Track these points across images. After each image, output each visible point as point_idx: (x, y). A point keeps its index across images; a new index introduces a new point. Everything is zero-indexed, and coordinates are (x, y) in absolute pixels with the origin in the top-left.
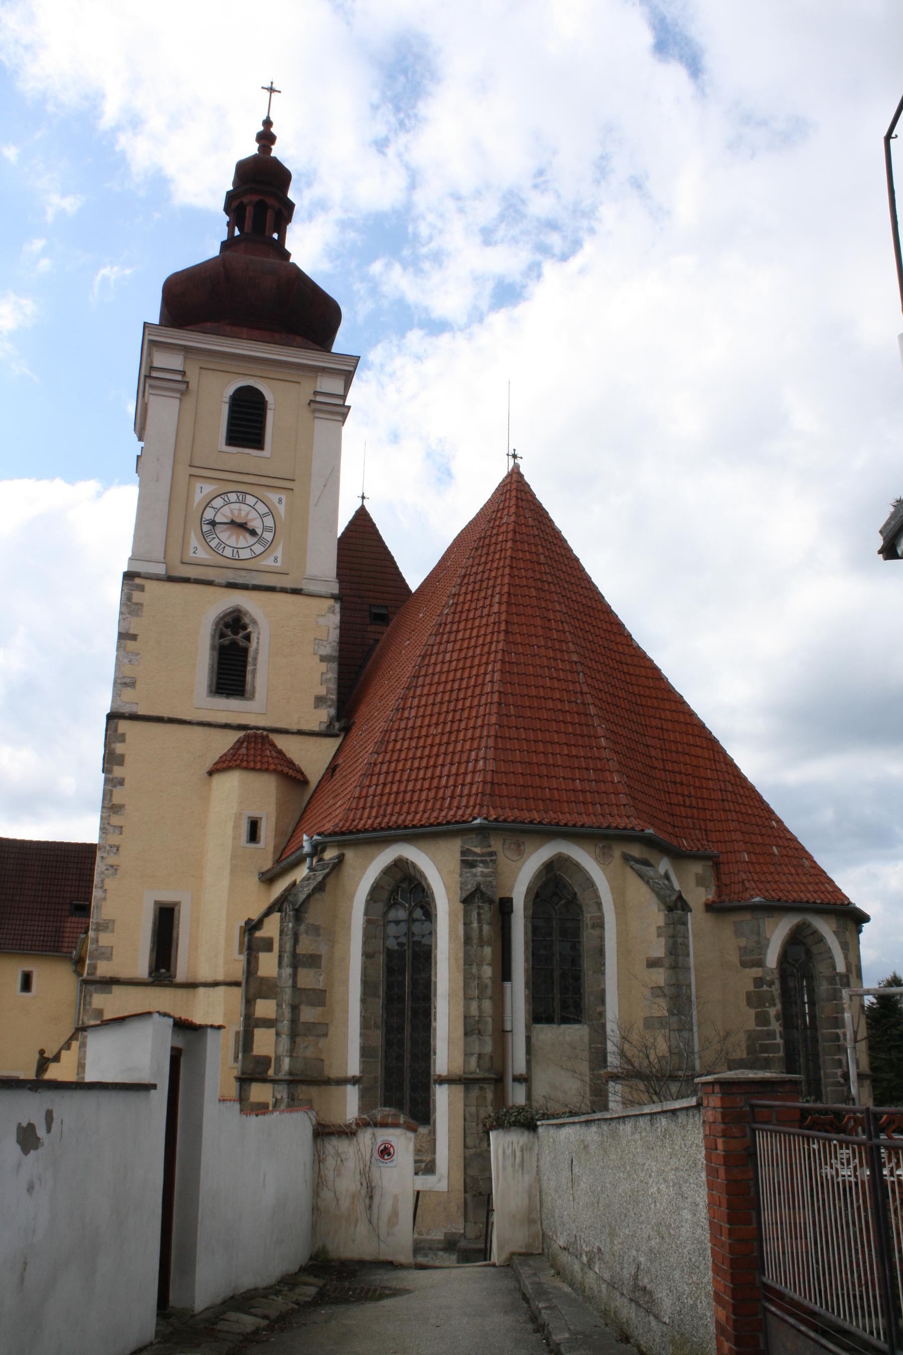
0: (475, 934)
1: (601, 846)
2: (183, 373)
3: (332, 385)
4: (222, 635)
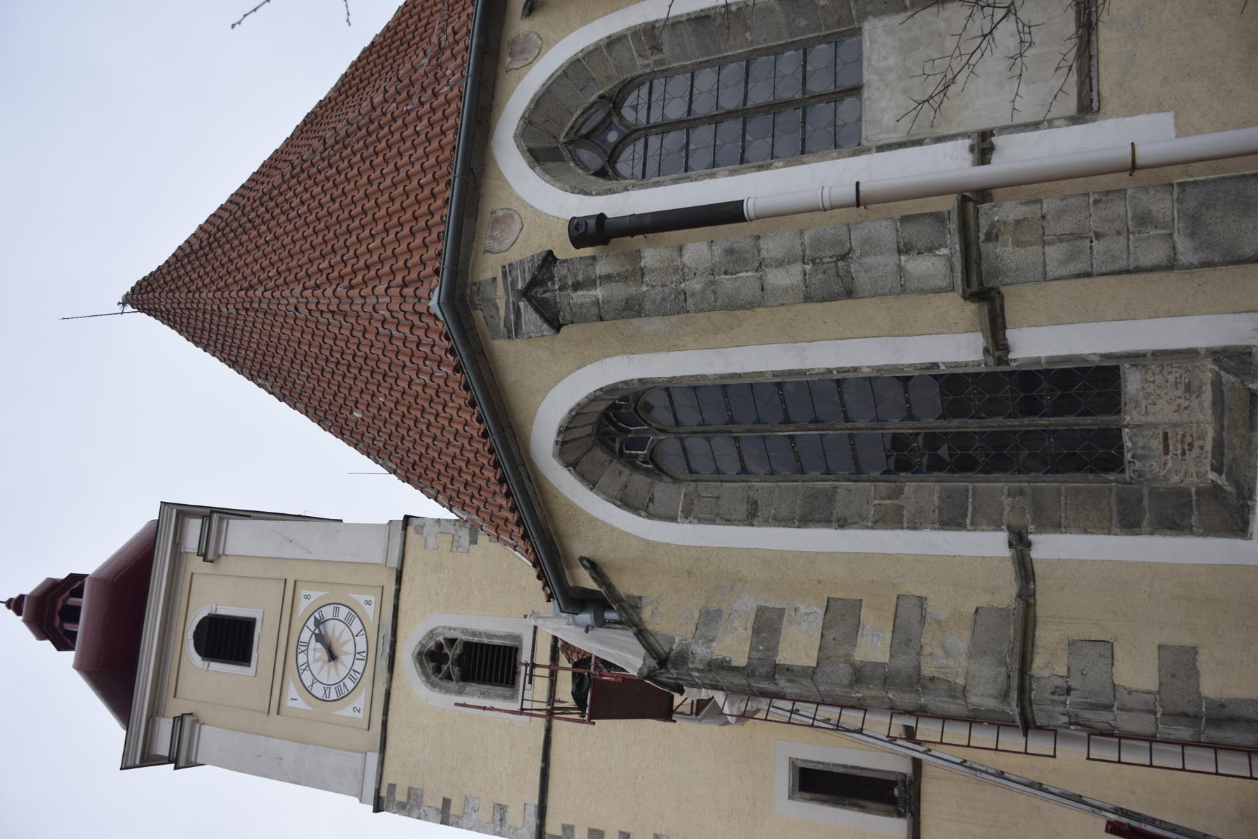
1: (509, 59)
4: (449, 677)
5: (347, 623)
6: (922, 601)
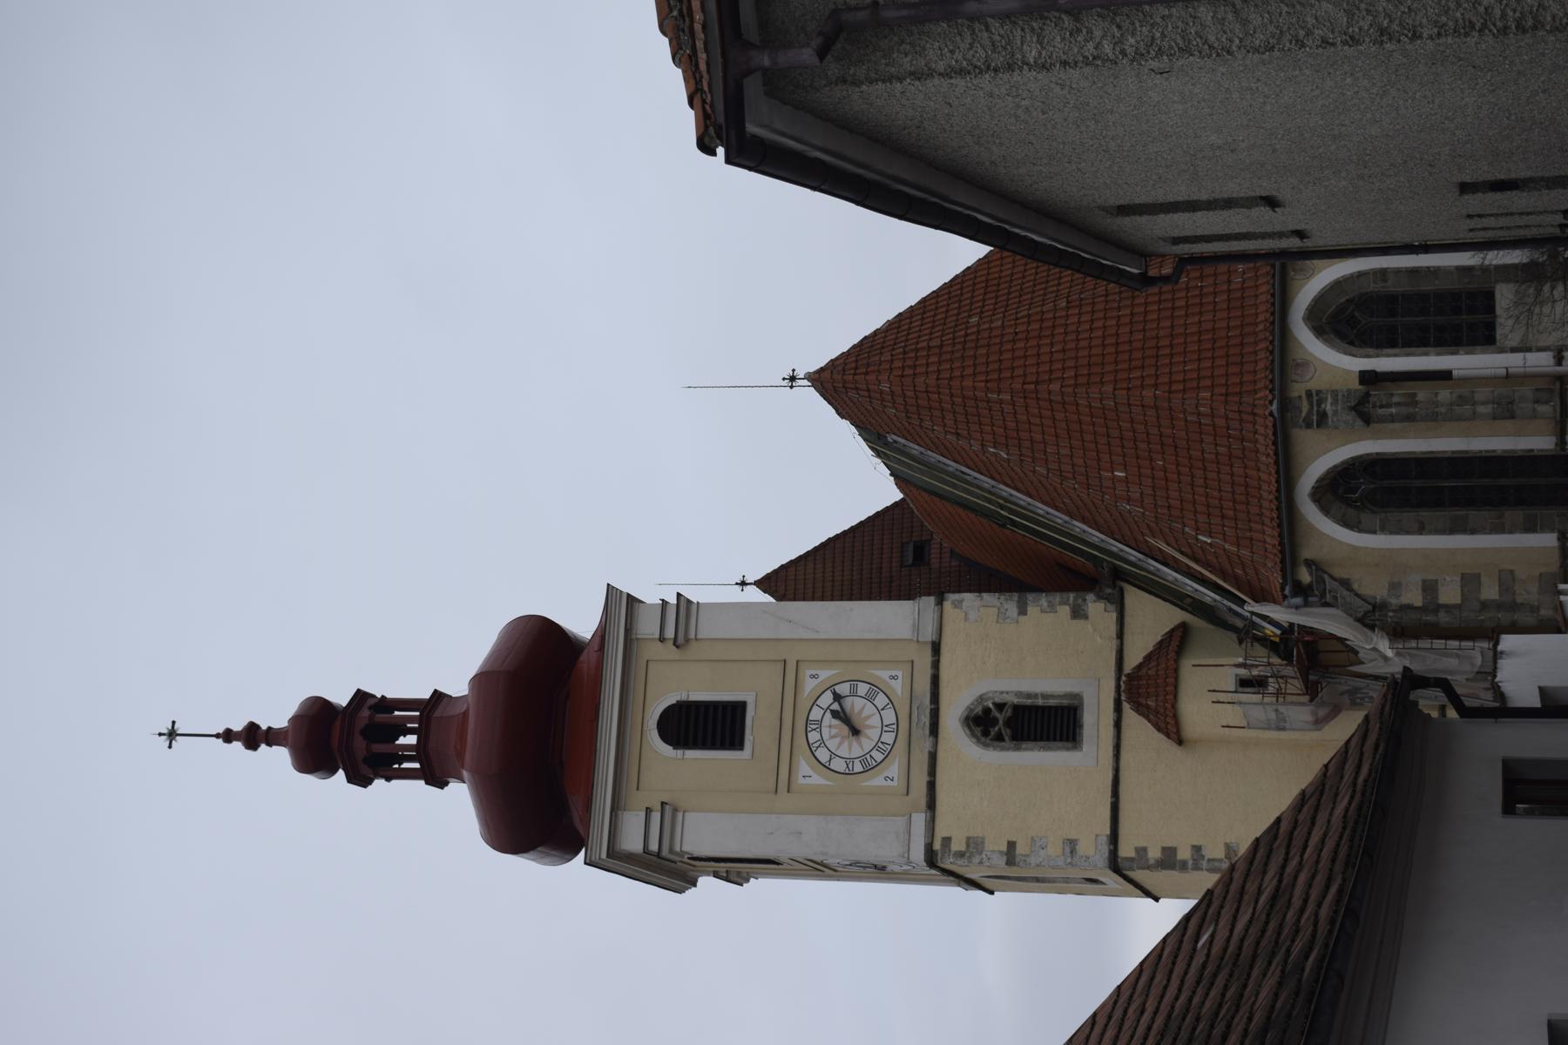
0: (1404, 410)
2: (648, 811)
3: (648, 627)
4: (999, 738)
5: (869, 698)
6: (1512, 572)
